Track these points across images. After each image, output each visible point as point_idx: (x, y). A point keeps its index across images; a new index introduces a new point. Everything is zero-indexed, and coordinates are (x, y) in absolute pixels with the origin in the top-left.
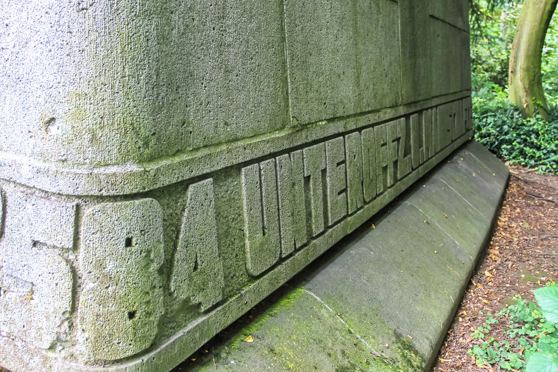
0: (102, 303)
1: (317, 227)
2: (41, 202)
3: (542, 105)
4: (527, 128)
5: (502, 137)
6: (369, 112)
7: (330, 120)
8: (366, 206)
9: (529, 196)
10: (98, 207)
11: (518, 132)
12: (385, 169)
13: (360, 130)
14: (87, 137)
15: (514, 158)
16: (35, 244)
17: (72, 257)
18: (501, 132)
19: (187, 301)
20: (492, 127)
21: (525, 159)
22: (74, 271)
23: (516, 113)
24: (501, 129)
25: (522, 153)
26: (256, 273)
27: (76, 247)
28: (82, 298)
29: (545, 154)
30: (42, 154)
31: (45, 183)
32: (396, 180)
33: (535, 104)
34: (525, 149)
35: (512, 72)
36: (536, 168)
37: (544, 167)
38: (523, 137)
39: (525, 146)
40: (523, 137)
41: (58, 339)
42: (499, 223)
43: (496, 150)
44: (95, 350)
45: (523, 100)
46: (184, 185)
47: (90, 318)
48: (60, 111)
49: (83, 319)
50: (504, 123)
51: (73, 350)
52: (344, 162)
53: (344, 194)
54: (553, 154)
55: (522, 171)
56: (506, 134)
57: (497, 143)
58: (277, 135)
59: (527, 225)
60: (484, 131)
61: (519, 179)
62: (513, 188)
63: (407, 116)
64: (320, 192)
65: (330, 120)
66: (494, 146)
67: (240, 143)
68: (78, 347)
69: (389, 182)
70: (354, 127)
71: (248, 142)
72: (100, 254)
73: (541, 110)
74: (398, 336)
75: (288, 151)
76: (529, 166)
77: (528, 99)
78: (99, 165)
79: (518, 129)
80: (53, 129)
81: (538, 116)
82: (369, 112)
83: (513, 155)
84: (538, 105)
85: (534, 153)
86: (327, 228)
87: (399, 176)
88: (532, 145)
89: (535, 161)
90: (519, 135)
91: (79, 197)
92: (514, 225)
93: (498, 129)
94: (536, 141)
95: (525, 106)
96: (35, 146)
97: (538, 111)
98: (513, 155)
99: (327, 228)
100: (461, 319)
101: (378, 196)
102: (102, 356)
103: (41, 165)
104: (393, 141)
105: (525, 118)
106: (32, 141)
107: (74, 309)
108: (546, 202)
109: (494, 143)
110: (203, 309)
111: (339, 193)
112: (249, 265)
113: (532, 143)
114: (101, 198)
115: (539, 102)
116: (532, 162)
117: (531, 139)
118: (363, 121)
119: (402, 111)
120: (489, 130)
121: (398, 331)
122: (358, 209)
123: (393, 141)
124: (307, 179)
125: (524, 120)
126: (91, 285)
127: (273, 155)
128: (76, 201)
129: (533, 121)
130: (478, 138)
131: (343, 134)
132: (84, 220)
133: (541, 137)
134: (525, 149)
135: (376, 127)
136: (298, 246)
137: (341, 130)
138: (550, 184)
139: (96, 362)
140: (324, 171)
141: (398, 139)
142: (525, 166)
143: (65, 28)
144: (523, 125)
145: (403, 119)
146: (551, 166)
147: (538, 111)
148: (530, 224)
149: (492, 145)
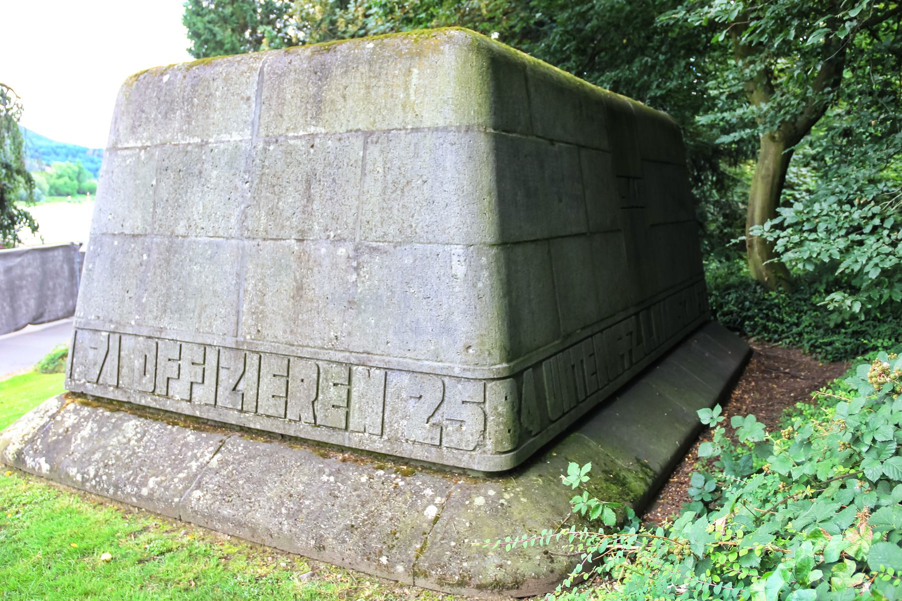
0: (498, 425)
1: (581, 397)
2: (466, 383)
3: (783, 277)
4: (768, 303)
5: (745, 314)
6: (607, 318)
7: (583, 328)
8: (611, 384)
9: (767, 370)
10: (494, 383)
11: (760, 307)
12: (622, 356)
13: (601, 331)
14: (487, 353)
15: (758, 334)
16: (463, 402)
17: (482, 406)
18: (743, 309)
19: (527, 428)
20: (733, 305)
21: (769, 334)
22: (484, 412)
23: (758, 287)
24: (743, 305)
25: (765, 328)
26: (553, 419)
27: (484, 402)
28: (488, 424)
29: (788, 328)
30: (466, 362)
31: (469, 375)
32: (631, 364)
33: (776, 276)
34: (767, 324)
35: (749, 246)
36: (780, 343)
37: (788, 341)
38: (765, 312)
39: (768, 321)
40: (765, 312)
41: (478, 445)
42: (733, 396)
43: (739, 327)
44: (496, 446)
45: (764, 273)
46: (522, 372)
47: (492, 432)
48: (474, 342)
49: (490, 433)
50: (746, 299)
51: (485, 449)
52: (593, 354)
53: (595, 375)
54: (794, 327)
55: (766, 346)
56: (749, 310)
57: (739, 320)
58: (556, 342)
59: (758, 396)
60: (725, 309)
61: (760, 355)
62: (753, 364)
63: (637, 314)
64: (581, 374)
65: (583, 328)
66: (737, 323)
67: (541, 349)
68: (487, 447)
69: (626, 365)
70: (597, 330)
71: (544, 348)
72: (495, 403)
73: (783, 282)
74: (638, 461)
75: (562, 351)
76: (773, 341)
77: (769, 272)
78: (492, 365)
79: (760, 304)
80: (471, 351)
81: (780, 289)
82: (607, 318)
83: (757, 331)
84: (780, 277)
85: (777, 327)
86: (587, 397)
87: (634, 361)
88: (776, 320)
89: (779, 335)
90: (761, 310)
91: (484, 379)
92: (746, 396)
93: (740, 306)
94: (777, 315)
95: (766, 279)
96: (461, 358)
97: (779, 284)
98: (757, 331)
99: (587, 397)
100: (687, 459)
101: (619, 376)
102: (499, 450)
103: (465, 367)
104: (627, 335)
105: (767, 292)
106: (460, 356)
107: (485, 429)
108: (782, 375)
109: (737, 320)
110: (533, 434)
111: (593, 375)
112: (550, 415)
113: (775, 317)
114: (493, 379)
115: (780, 274)
116: (776, 336)
117: (773, 313)
118: (603, 325)
119: (632, 311)
120: (730, 308)
121: (639, 457)
122: (605, 386)
123: (627, 335)
124: (573, 366)
125: (766, 294)
126: (492, 418)
127: (555, 354)
128: (483, 382)
129: (774, 294)
130: (720, 316)
131: (591, 336)
132: (488, 389)
133: (783, 311)
134: (767, 324)
135: (612, 328)
136: (572, 406)
137: (590, 333)
138: (792, 357)
139: (496, 454)
140: (582, 361)
141: (631, 333)
142: (769, 341)
143: (473, 306)
144: (764, 299)
145: (633, 317)
146: (794, 338)
147: (779, 284)
148: (761, 394)
149: (735, 322)
